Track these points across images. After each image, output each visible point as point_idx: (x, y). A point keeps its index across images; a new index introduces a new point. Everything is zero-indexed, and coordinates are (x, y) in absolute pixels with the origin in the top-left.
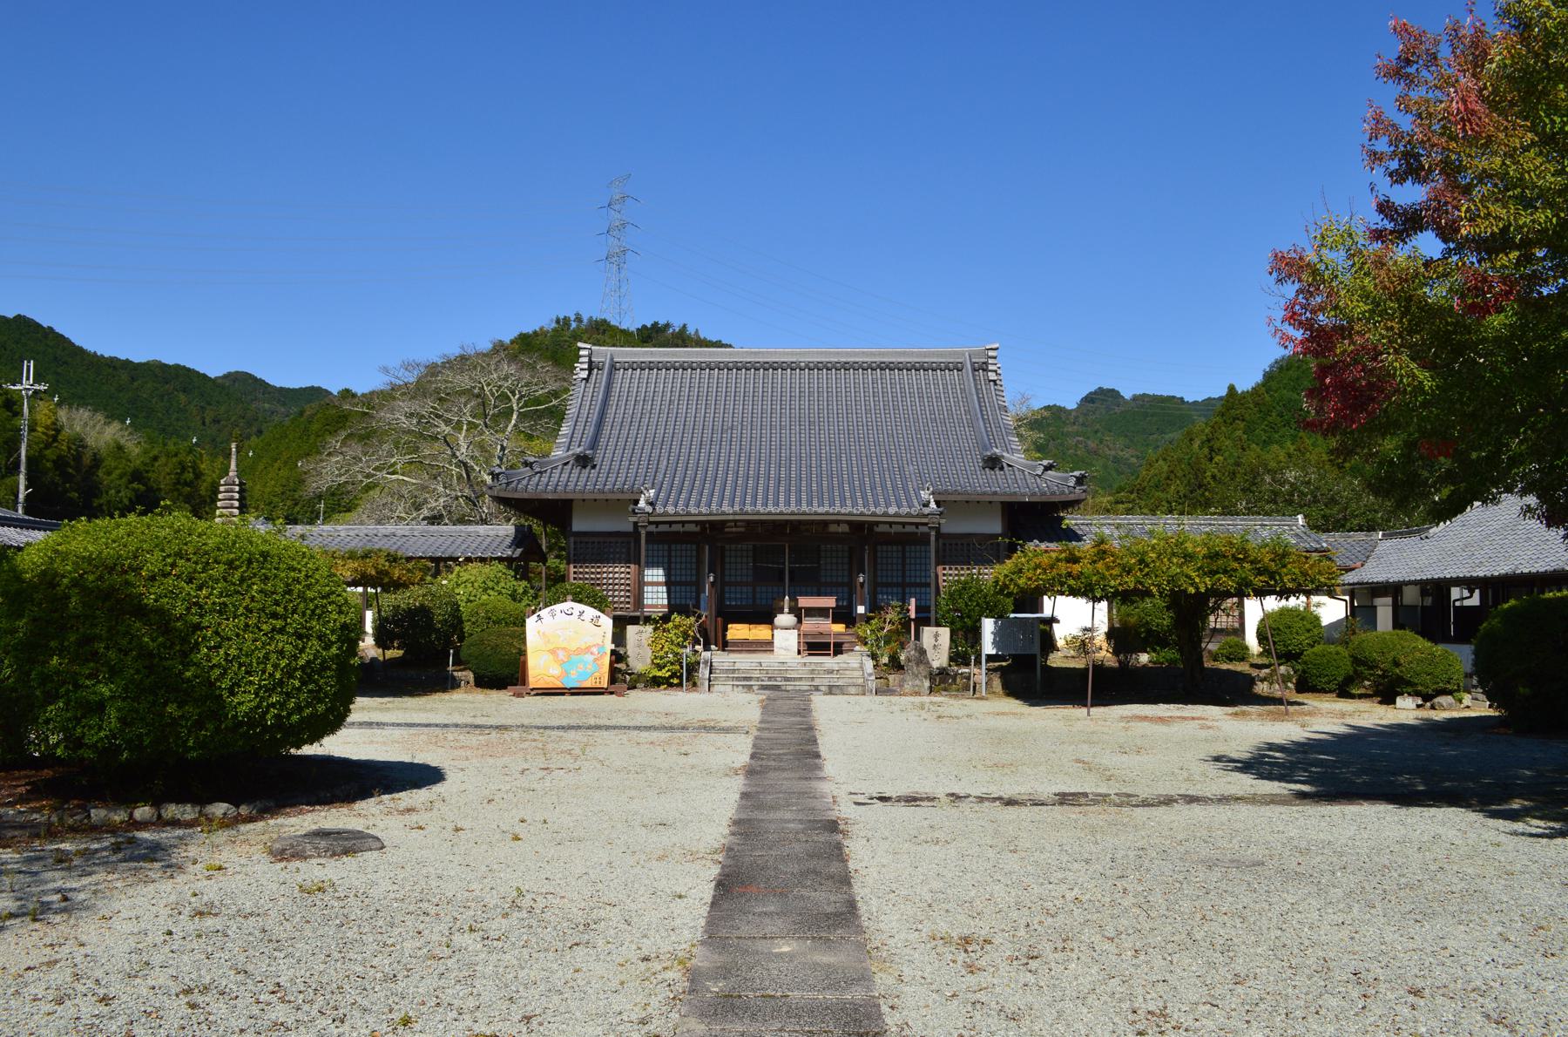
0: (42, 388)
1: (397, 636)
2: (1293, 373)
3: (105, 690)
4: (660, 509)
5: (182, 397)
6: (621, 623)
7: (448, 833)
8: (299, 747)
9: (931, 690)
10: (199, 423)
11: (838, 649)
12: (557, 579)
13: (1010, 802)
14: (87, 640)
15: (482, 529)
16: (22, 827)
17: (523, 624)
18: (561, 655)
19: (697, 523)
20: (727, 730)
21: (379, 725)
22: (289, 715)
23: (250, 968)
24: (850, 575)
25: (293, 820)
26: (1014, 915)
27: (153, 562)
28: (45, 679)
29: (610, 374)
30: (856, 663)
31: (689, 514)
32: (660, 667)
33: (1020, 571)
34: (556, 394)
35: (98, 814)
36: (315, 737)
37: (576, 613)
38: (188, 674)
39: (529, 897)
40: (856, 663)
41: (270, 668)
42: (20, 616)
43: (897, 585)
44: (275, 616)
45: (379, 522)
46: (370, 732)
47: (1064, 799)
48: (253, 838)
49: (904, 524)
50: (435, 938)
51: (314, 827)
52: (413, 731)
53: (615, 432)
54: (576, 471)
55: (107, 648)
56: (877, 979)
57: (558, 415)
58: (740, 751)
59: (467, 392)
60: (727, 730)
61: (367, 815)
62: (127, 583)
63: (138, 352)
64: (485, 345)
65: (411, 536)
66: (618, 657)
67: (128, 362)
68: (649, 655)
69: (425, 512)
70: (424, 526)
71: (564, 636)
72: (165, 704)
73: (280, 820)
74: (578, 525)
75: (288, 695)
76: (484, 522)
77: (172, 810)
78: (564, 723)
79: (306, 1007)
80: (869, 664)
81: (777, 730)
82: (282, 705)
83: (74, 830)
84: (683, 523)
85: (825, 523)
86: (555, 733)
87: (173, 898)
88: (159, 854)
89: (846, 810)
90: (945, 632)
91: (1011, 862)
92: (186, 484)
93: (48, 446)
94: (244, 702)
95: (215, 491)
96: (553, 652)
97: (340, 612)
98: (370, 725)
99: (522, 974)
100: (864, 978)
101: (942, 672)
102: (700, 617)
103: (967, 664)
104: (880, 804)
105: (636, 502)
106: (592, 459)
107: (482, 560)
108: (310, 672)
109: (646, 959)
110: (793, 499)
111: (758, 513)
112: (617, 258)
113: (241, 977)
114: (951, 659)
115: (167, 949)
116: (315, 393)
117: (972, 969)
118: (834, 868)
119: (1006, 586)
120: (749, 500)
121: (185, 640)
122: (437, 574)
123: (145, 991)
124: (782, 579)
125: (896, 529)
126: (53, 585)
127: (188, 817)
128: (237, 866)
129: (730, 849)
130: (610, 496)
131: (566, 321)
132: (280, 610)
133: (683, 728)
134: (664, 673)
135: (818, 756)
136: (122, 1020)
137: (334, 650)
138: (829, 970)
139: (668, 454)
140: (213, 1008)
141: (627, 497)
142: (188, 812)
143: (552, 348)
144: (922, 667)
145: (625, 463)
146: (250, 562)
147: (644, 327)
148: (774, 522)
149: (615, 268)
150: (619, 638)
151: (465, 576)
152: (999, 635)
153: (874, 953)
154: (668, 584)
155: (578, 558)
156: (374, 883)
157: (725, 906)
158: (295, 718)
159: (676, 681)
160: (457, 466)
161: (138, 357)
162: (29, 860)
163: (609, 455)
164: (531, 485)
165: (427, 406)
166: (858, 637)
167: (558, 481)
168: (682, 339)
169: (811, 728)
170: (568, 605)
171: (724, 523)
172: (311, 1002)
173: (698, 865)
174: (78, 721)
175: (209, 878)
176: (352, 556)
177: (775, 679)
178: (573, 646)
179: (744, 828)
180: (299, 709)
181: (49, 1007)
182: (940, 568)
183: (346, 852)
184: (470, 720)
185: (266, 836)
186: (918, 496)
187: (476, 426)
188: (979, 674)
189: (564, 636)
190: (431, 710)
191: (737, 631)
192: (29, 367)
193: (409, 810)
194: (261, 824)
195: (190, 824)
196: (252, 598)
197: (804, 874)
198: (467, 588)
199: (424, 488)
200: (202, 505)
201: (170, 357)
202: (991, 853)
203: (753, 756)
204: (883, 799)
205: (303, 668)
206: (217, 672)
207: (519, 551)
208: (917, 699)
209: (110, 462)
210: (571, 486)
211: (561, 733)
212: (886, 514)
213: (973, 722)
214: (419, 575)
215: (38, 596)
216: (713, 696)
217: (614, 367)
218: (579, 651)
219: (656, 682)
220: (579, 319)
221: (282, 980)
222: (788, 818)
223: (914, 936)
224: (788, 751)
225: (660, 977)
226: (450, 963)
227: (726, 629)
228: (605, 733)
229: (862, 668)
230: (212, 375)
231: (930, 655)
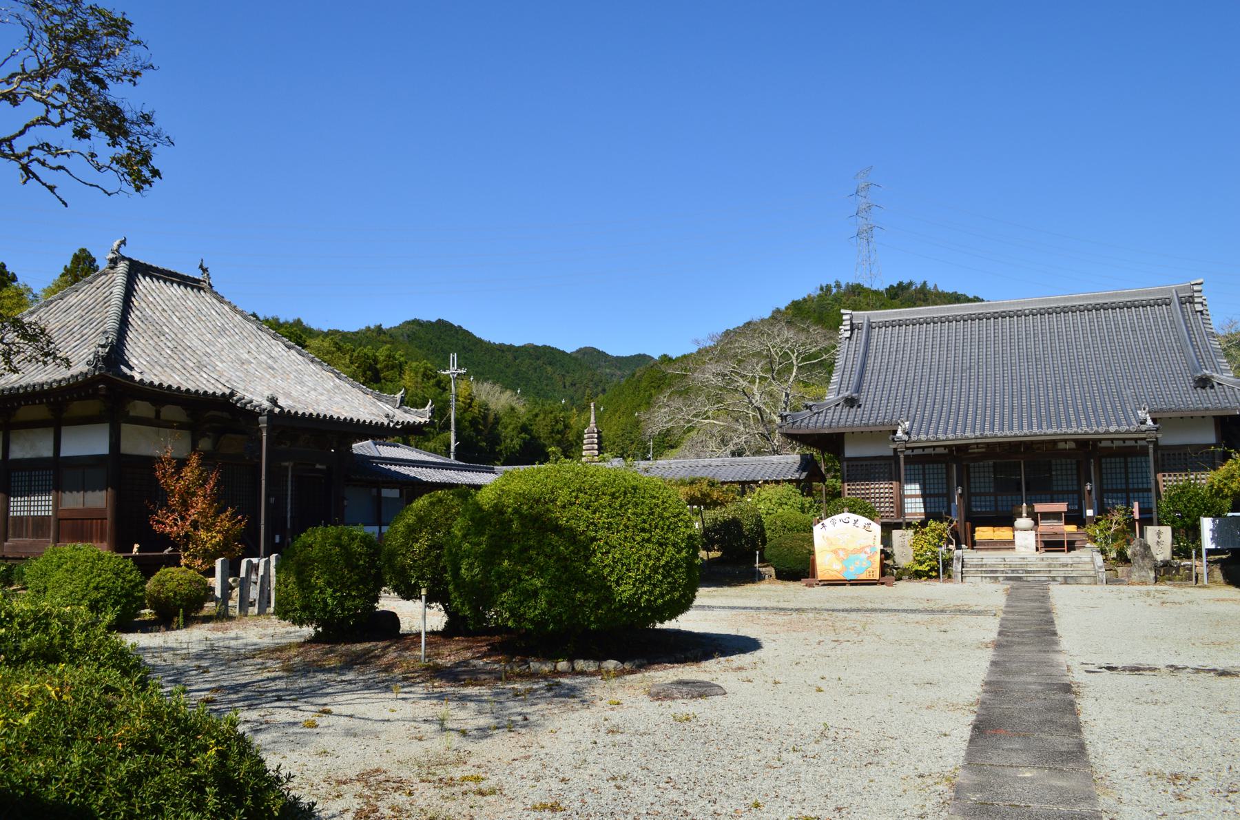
0: (463, 371)
1: (717, 541)
3: (537, 583)
4: (914, 437)
5: (549, 369)
6: (887, 528)
7: (770, 685)
8: (662, 622)
9: (1156, 580)
10: (568, 390)
11: (1071, 546)
12: (835, 494)
13: (1224, 673)
14: (525, 549)
15: (775, 458)
16: (490, 672)
17: (811, 530)
18: (842, 554)
19: (945, 447)
20: (978, 613)
22: (656, 599)
23: (650, 767)
24: (1079, 484)
25: (660, 673)
26: (1220, 760)
27: (563, 496)
28: (500, 576)
29: (868, 332)
30: (1088, 557)
31: (938, 440)
32: (921, 563)
33: (1233, 476)
34: (826, 350)
35: (534, 665)
36: (673, 615)
37: (852, 521)
38: (589, 571)
39: (833, 730)
40: (1088, 557)
41: (642, 567)
42: (483, 534)
44: (643, 530)
45: (698, 456)
46: (710, 612)
48: (637, 685)
49: (1124, 440)
50: (770, 754)
51: (676, 679)
52: (734, 612)
53: (875, 378)
54: (846, 410)
55: (538, 554)
56: (1101, 799)
57: (829, 367)
58: (990, 629)
59: (758, 354)
60: (978, 613)
61: (709, 670)
62: (548, 510)
63: (517, 340)
64: (767, 315)
65: (719, 465)
66: (886, 555)
67: (511, 346)
68: (911, 553)
69: (731, 447)
70: (730, 459)
71: (844, 540)
72: (576, 592)
73: (652, 673)
74: (849, 452)
75: (655, 586)
76: (776, 452)
77: (580, 664)
78: (847, 606)
79: (690, 793)
80: (1099, 559)
81: (1020, 613)
82: (651, 593)
83: (521, 676)
84: (934, 447)
85: (1055, 442)
86: (841, 614)
87: (592, 721)
88: (577, 693)
89: (1078, 676)
90: (1167, 531)
91: (1221, 720)
92: (558, 432)
93: (465, 411)
94: (625, 591)
95: (580, 437)
96: (835, 552)
97: (687, 527)
99: (832, 781)
100: (1090, 798)
101: (1166, 564)
102: (951, 522)
103: (1189, 558)
104: (1108, 672)
105: (895, 432)
106: (858, 400)
107: (777, 482)
108: (668, 569)
109: (921, 776)
110: (1025, 424)
111: (996, 437)
112: (865, 234)
113: (645, 772)
114: (1174, 553)
115: (595, 752)
116: (641, 359)
117: (1179, 798)
118: (1068, 719)
119: (1220, 490)
120: (987, 425)
121: (586, 548)
122: (743, 493)
123: (587, 777)
124: (1020, 489)
125: (1116, 444)
126: (502, 513)
127: (592, 669)
128: (626, 704)
129: (983, 703)
130: (873, 429)
131: (828, 288)
132: (647, 526)
133: (942, 611)
134: (925, 568)
135: (1055, 634)
136: (577, 793)
137: (684, 554)
138: (1062, 791)
139: (917, 388)
140: (631, 789)
141: (887, 428)
142: (591, 666)
143: (818, 312)
144: (1147, 560)
145: (884, 402)
146: (625, 493)
147: (892, 286)
148: (1010, 443)
149: (865, 241)
150: (886, 540)
151: (764, 494)
152: (1218, 534)
153: (1099, 782)
154: (924, 496)
155: (850, 478)
156: (722, 717)
157: (981, 743)
158: (660, 601)
159: (934, 574)
160: (754, 410)
161: (518, 342)
162: (497, 694)
163: (871, 396)
164: (811, 423)
165: (728, 367)
166: (1089, 536)
167: (831, 419)
168: (924, 296)
169: (1049, 612)
170: (845, 515)
171: (967, 446)
172: (693, 790)
173: (958, 714)
174: (521, 603)
175: (612, 709)
176: (683, 483)
178: (851, 547)
179: (994, 687)
180: (662, 595)
181: (531, 783)
182: (1159, 476)
183: (701, 696)
184: (775, 605)
185: (644, 685)
186: (1136, 415)
187: (766, 379)
188: (1201, 566)
189: (844, 540)
190: (746, 597)
191: (983, 533)
192: (454, 356)
193: (740, 669)
194: (639, 676)
195: (592, 674)
196: (629, 519)
197: (1043, 723)
198: (762, 502)
199: (728, 428)
200: (570, 449)
201: (539, 340)
202: (1203, 713)
203: (1000, 634)
204: (1110, 668)
205: (664, 566)
206: (607, 570)
207: (805, 474)
208: (1144, 588)
209: (506, 420)
210: (842, 422)
211: (845, 614)
212: (1107, 432)
213: (1194, 607)
214: (731, 495)
215: (493, 521)
216: (966, 586)
218: (856, 551)
219: (918, 575)
220: (838, 285)
221: (672, 775)
222: (1030, 680)
223: (1132, 771)
224: (1030, 628)
225: (932, 789)
226: (782, 771)
227: (973, 531)
228: (880, 615)
229: (1093, 562)
230: (568, 351)
231: (1154, 549)
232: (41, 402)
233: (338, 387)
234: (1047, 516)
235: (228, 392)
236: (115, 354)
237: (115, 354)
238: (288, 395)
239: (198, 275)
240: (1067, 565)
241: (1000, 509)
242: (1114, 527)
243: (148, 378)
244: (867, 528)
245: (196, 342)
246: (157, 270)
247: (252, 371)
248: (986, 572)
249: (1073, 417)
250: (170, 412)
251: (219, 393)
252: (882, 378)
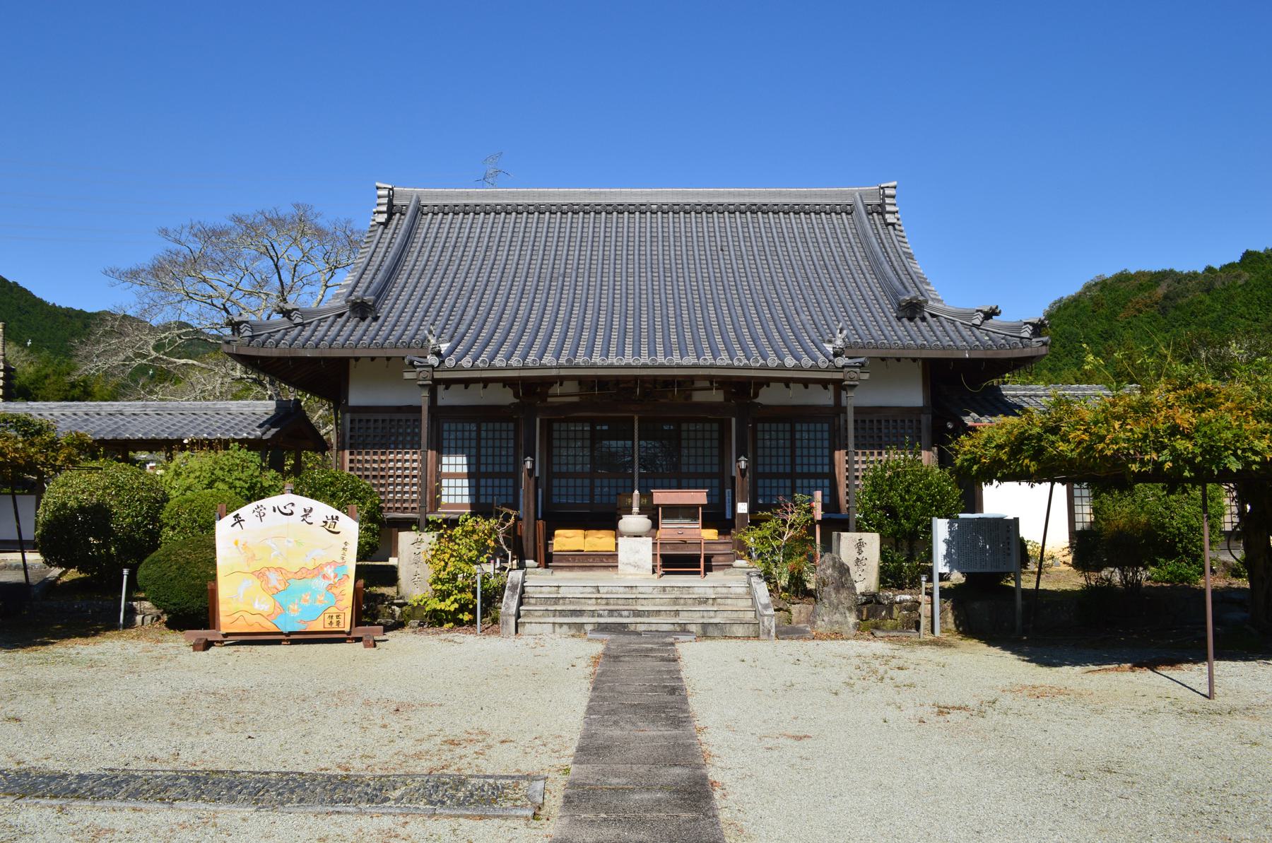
2: (1071, 311)
17: (209, 527)
18: (274, 578)
30: (736, 585)
32: (444, 596)
37: (299, 512)
40: (736, 585)
53: (412, 281)
68: (428, 573)
74: (356, 398)
80: (762, 589)
90: (872, 541)
96: (260, 574)
111: (594, 367)
130: (390, 353)
134: (449, 605)
144: (844, 594)
155: (354, 440)
159: (466, 617)
177: (618, 613)
191: (566, 540)
216: (525, 640)
217: (419, 210)
219: (436, 619)
224: (640, 682)
227: (550, 536)
229: (751, 593)
234: (674, 511)
240: (704, 601)
241: (597, 499)
242: (789, 533)
244: (330, 526)
248: (562, 613)
252: (424, 281)
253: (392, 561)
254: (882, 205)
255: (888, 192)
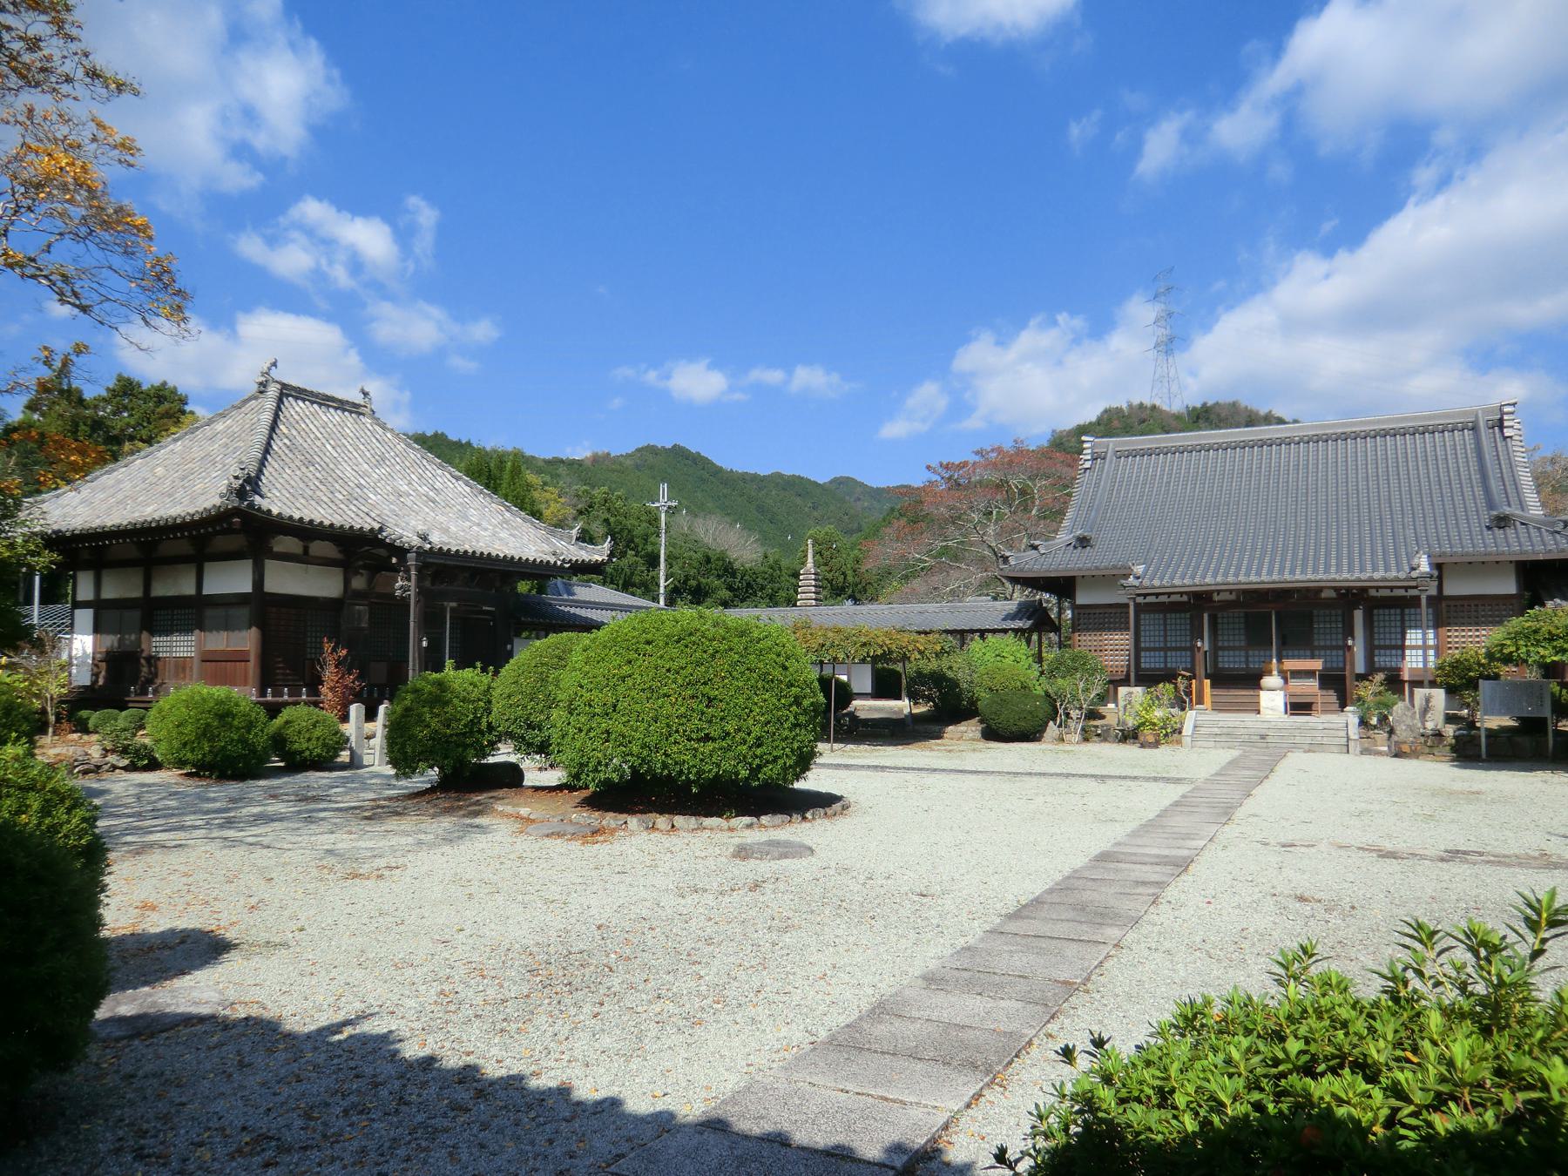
21: (883, 768)
43: (1160, 649)
47: (1453, 855)
63: (762, 468)
74: (1081, 599)
98: (838, 767)
110: (1345, 568)
232: (183, 537)
233: (506, 522)
234: (1297, 674)
235: (377, 526)
236: (250, 484)
237: (250, 484)
238: (446, 531)
239: (359, 399)
243: (287, 512)
245: (349, 472)
246: (317, 395)
247: (409, 503)
249: (1333, 562)
250: (320, 548)
251: (367, 527)
253: (449, 663)
254: (1501, 420)
255: (1506, 409)
